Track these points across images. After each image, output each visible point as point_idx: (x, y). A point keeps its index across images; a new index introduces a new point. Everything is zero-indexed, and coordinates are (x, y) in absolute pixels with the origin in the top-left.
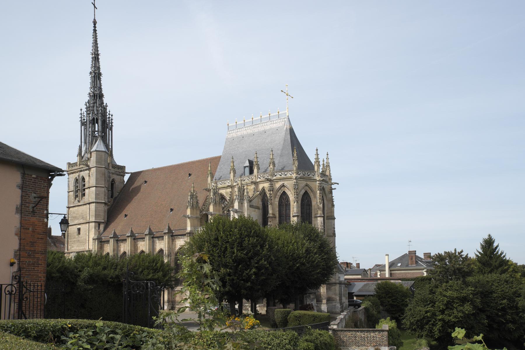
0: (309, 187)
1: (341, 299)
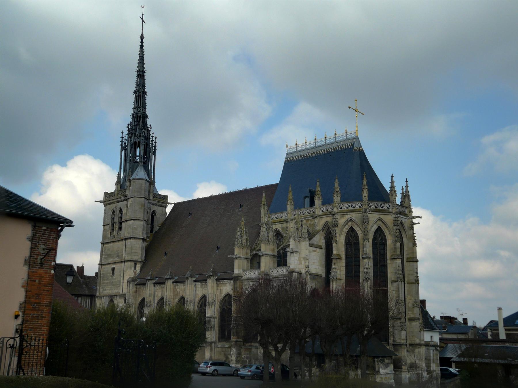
0: (383, 222)
1: (428, 366)
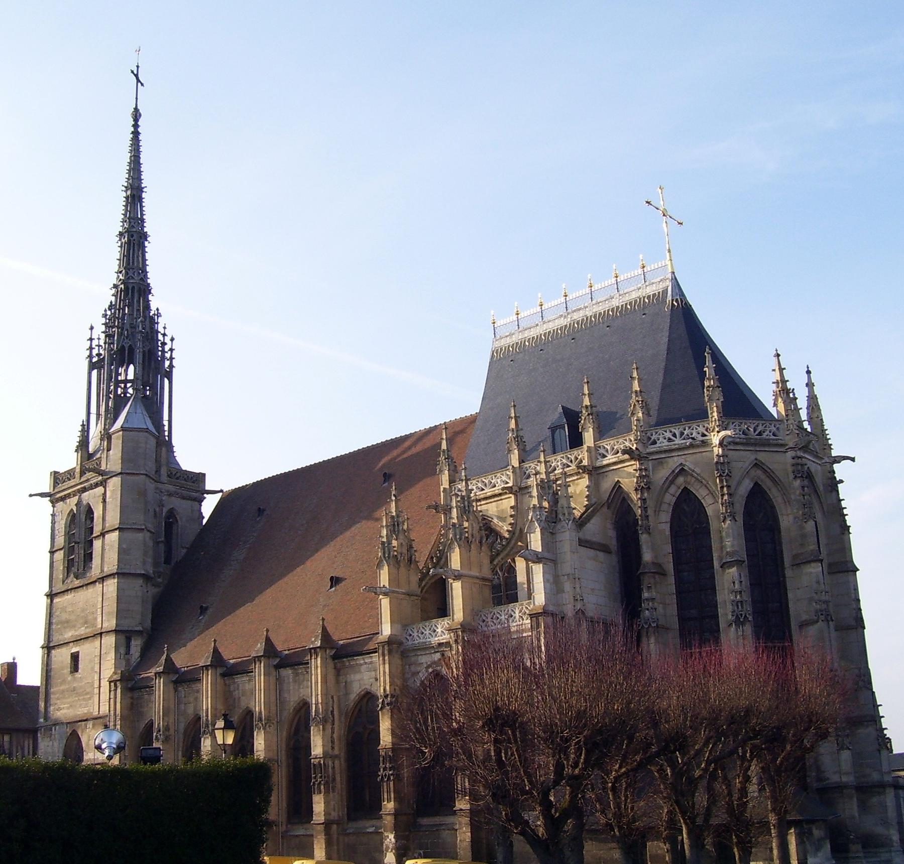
0: (765, 471)
